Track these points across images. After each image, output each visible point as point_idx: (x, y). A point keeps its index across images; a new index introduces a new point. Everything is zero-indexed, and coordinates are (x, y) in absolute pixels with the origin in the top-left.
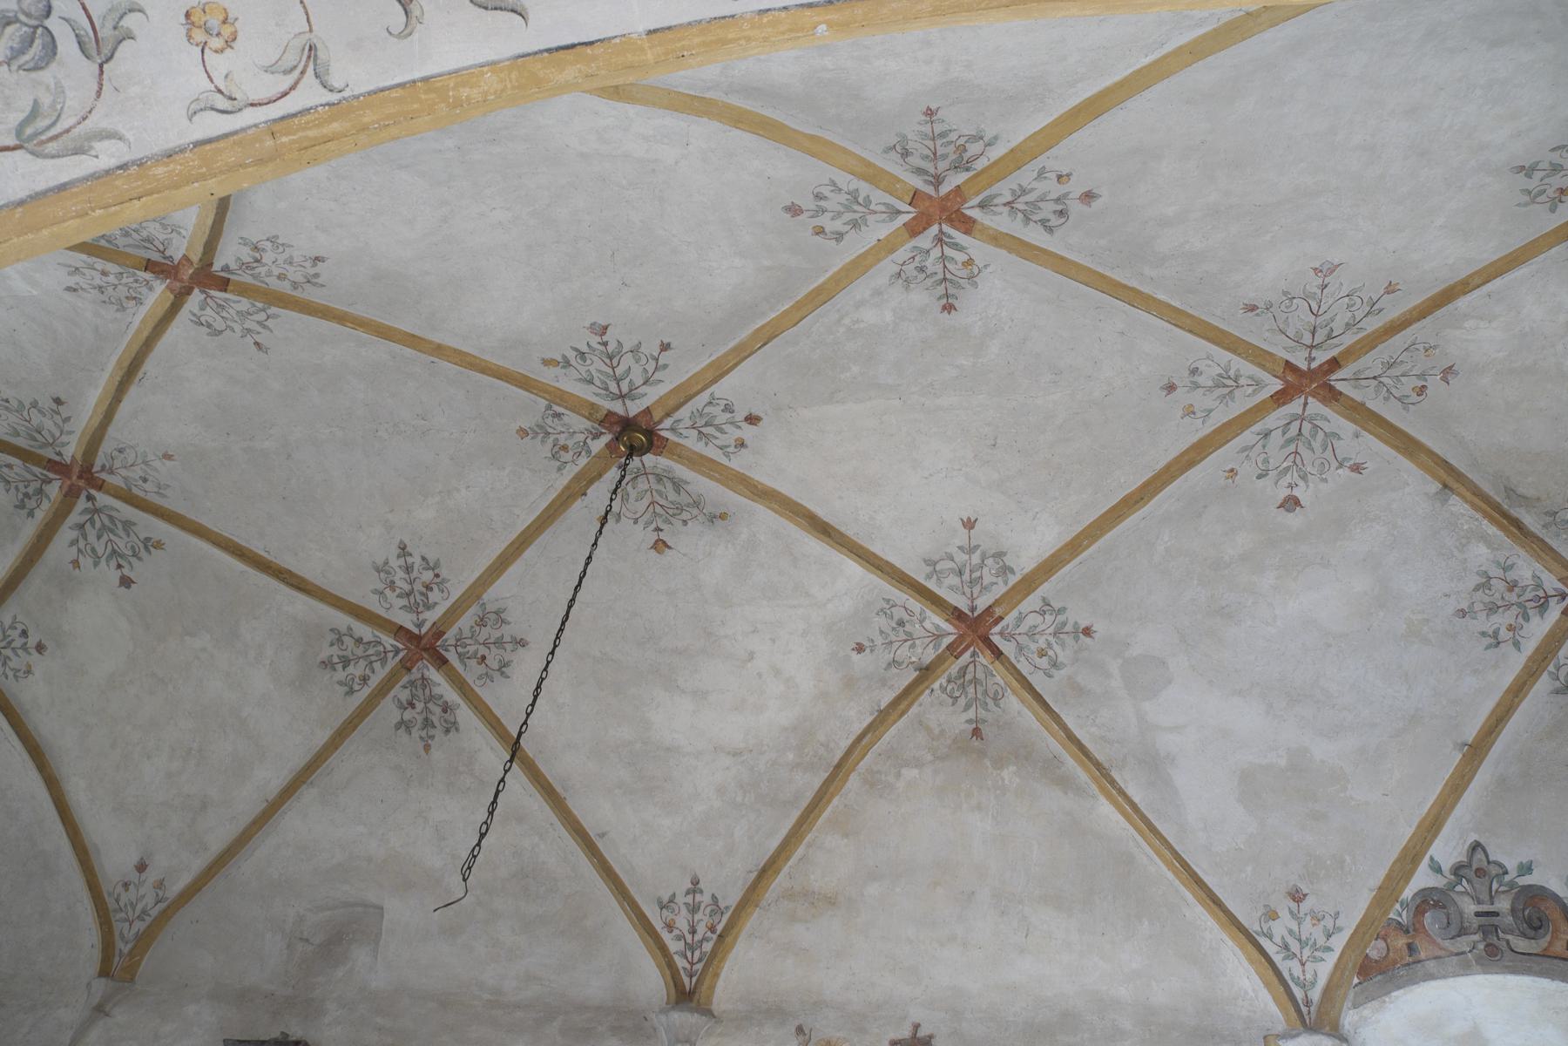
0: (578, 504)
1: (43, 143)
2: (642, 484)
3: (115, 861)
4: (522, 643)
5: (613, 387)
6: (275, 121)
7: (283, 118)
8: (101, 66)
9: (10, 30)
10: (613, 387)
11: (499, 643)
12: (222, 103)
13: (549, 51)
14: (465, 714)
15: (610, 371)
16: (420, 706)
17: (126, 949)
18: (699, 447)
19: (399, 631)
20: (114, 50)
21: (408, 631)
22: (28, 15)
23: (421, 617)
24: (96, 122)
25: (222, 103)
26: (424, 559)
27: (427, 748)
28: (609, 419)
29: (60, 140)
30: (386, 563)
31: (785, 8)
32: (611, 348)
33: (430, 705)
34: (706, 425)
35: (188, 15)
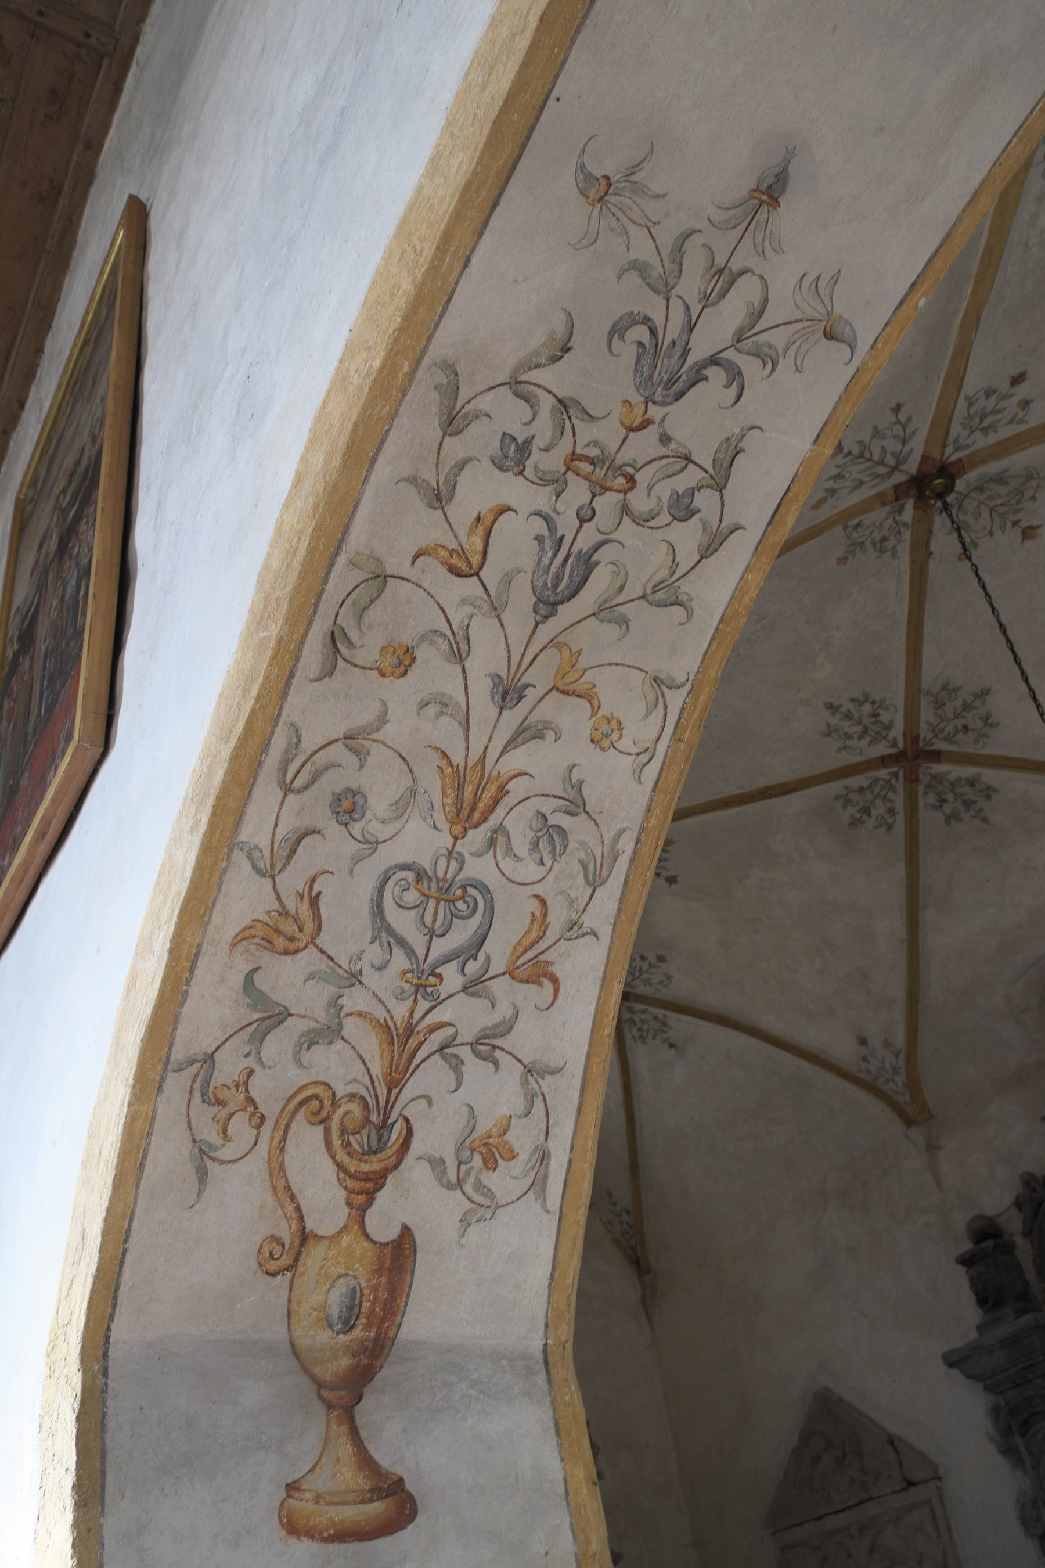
0: (932, 564)
1: (600, 874)
2: (970, 506)
3: (843, 1049)
4: (984, 693)
5: (882, 470)
6: (674, 733)
7: (676, 727)
8: (585, 811)
9: (541, 845)
10: (882, 470)
11: (967, 707)
12: (644, 758)
13: (769, 524)
14: (989, 776)
15: (869, 464)
16: (950, 797)
17: (907, 1098)
18: (992, 439)
19: (883, 761)
20: (582, 797)
21: (890, 756)
22: (540, 830)
23: (890, 737)
24: (608, 838)
25: (644, 758)
26: (852, 700)
27: (985, 820)
28: (900, 492)
29: (605, 864)
30: (829, 726)
31: (886, 325)
32: (856, 451)
33: (957, 790)
34: (982, 420)
35: (592, 741)
